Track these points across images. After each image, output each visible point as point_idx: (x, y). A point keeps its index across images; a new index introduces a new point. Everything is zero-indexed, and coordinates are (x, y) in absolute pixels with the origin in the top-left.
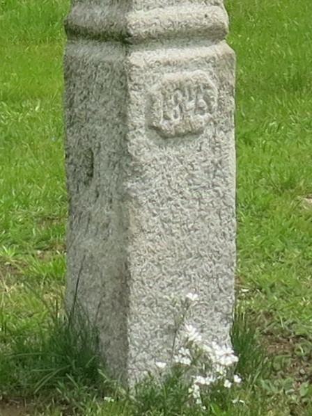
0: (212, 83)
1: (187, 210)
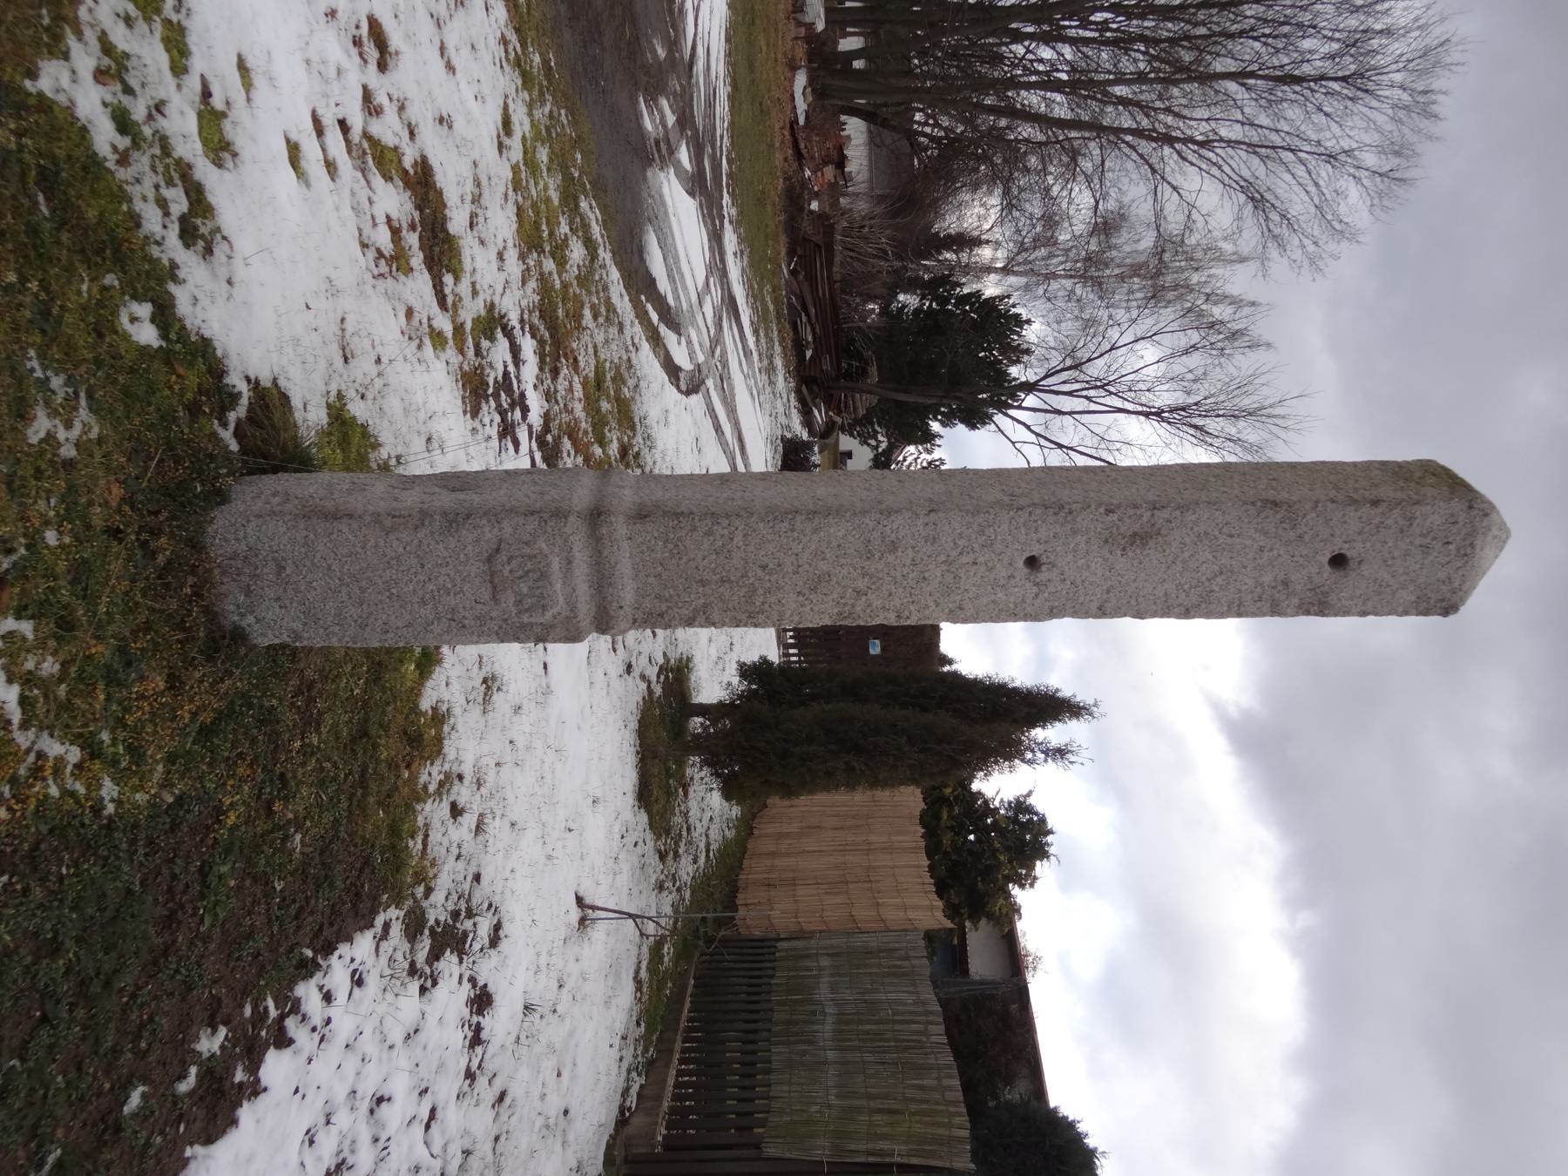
0: (549, 615)
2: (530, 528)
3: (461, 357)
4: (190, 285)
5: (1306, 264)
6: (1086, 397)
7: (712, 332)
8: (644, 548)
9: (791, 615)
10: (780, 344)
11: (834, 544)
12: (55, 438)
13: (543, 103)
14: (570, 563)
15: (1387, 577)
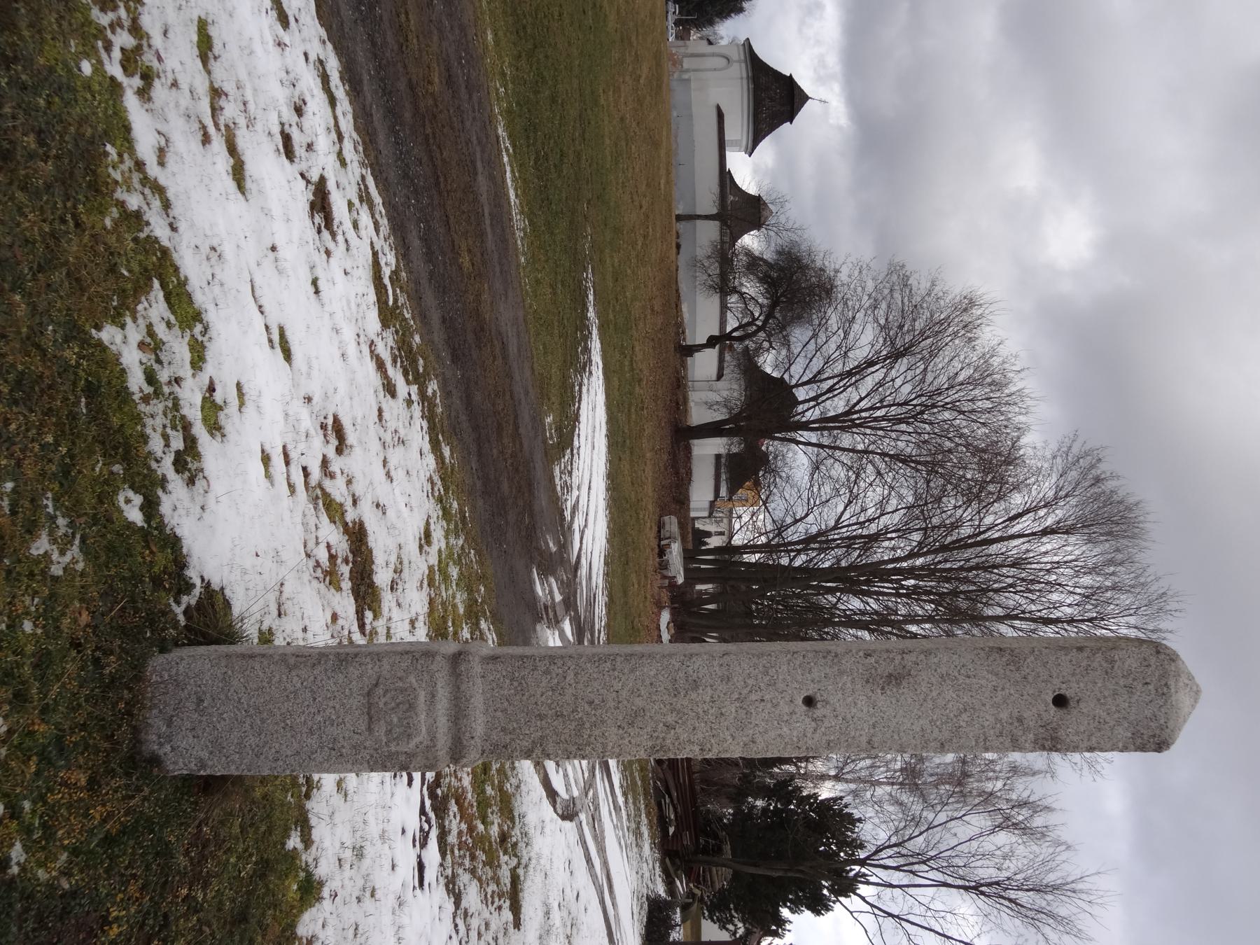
0: (412, 744)
2: (404, 665)
4: (174, 496)
5: (1086, 767)
6: (911, 872)
7: (586, 775)
8: (494, 685)
9: (613, 748)
10: (647, 817)
11: (648, 682)
12: (50, 558)
13: (457, 536)
14: (433, 696)
15: (1104, 715)
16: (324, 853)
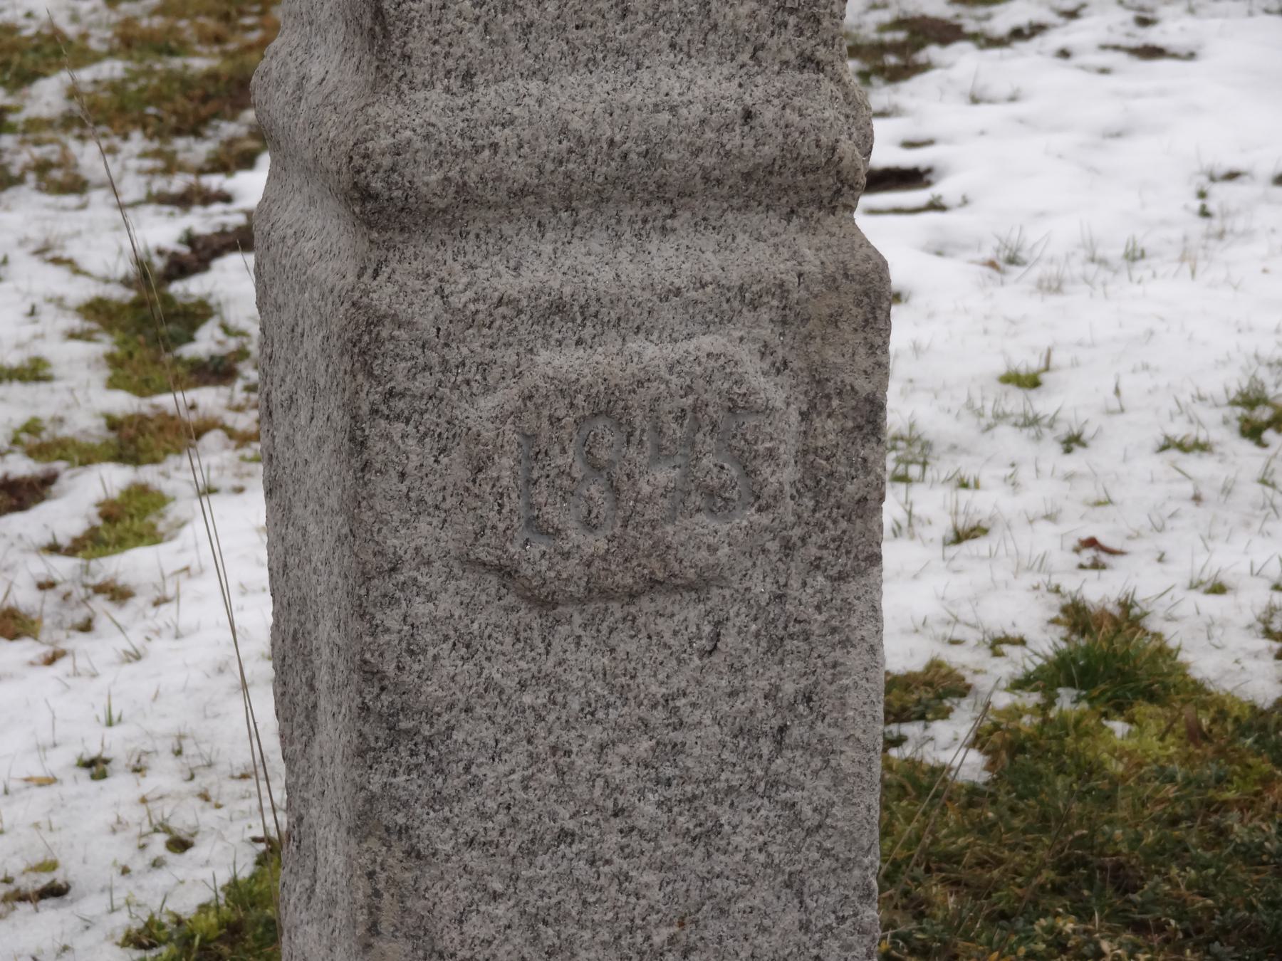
0: (772, 391)
1: (650, 877)
2: (416, 454)
3: (213, 439)
14: (559, 308)
16: (966, 612)
